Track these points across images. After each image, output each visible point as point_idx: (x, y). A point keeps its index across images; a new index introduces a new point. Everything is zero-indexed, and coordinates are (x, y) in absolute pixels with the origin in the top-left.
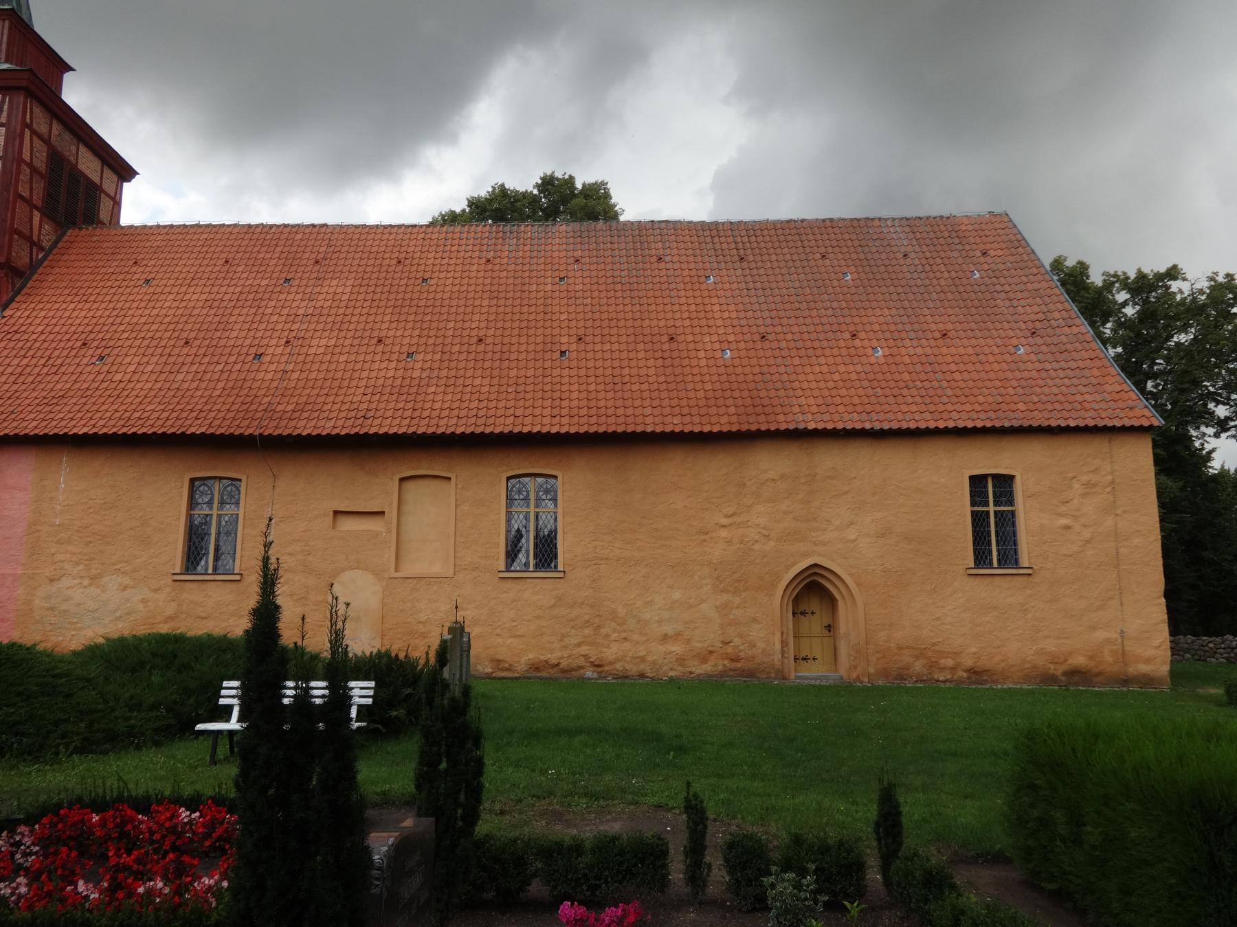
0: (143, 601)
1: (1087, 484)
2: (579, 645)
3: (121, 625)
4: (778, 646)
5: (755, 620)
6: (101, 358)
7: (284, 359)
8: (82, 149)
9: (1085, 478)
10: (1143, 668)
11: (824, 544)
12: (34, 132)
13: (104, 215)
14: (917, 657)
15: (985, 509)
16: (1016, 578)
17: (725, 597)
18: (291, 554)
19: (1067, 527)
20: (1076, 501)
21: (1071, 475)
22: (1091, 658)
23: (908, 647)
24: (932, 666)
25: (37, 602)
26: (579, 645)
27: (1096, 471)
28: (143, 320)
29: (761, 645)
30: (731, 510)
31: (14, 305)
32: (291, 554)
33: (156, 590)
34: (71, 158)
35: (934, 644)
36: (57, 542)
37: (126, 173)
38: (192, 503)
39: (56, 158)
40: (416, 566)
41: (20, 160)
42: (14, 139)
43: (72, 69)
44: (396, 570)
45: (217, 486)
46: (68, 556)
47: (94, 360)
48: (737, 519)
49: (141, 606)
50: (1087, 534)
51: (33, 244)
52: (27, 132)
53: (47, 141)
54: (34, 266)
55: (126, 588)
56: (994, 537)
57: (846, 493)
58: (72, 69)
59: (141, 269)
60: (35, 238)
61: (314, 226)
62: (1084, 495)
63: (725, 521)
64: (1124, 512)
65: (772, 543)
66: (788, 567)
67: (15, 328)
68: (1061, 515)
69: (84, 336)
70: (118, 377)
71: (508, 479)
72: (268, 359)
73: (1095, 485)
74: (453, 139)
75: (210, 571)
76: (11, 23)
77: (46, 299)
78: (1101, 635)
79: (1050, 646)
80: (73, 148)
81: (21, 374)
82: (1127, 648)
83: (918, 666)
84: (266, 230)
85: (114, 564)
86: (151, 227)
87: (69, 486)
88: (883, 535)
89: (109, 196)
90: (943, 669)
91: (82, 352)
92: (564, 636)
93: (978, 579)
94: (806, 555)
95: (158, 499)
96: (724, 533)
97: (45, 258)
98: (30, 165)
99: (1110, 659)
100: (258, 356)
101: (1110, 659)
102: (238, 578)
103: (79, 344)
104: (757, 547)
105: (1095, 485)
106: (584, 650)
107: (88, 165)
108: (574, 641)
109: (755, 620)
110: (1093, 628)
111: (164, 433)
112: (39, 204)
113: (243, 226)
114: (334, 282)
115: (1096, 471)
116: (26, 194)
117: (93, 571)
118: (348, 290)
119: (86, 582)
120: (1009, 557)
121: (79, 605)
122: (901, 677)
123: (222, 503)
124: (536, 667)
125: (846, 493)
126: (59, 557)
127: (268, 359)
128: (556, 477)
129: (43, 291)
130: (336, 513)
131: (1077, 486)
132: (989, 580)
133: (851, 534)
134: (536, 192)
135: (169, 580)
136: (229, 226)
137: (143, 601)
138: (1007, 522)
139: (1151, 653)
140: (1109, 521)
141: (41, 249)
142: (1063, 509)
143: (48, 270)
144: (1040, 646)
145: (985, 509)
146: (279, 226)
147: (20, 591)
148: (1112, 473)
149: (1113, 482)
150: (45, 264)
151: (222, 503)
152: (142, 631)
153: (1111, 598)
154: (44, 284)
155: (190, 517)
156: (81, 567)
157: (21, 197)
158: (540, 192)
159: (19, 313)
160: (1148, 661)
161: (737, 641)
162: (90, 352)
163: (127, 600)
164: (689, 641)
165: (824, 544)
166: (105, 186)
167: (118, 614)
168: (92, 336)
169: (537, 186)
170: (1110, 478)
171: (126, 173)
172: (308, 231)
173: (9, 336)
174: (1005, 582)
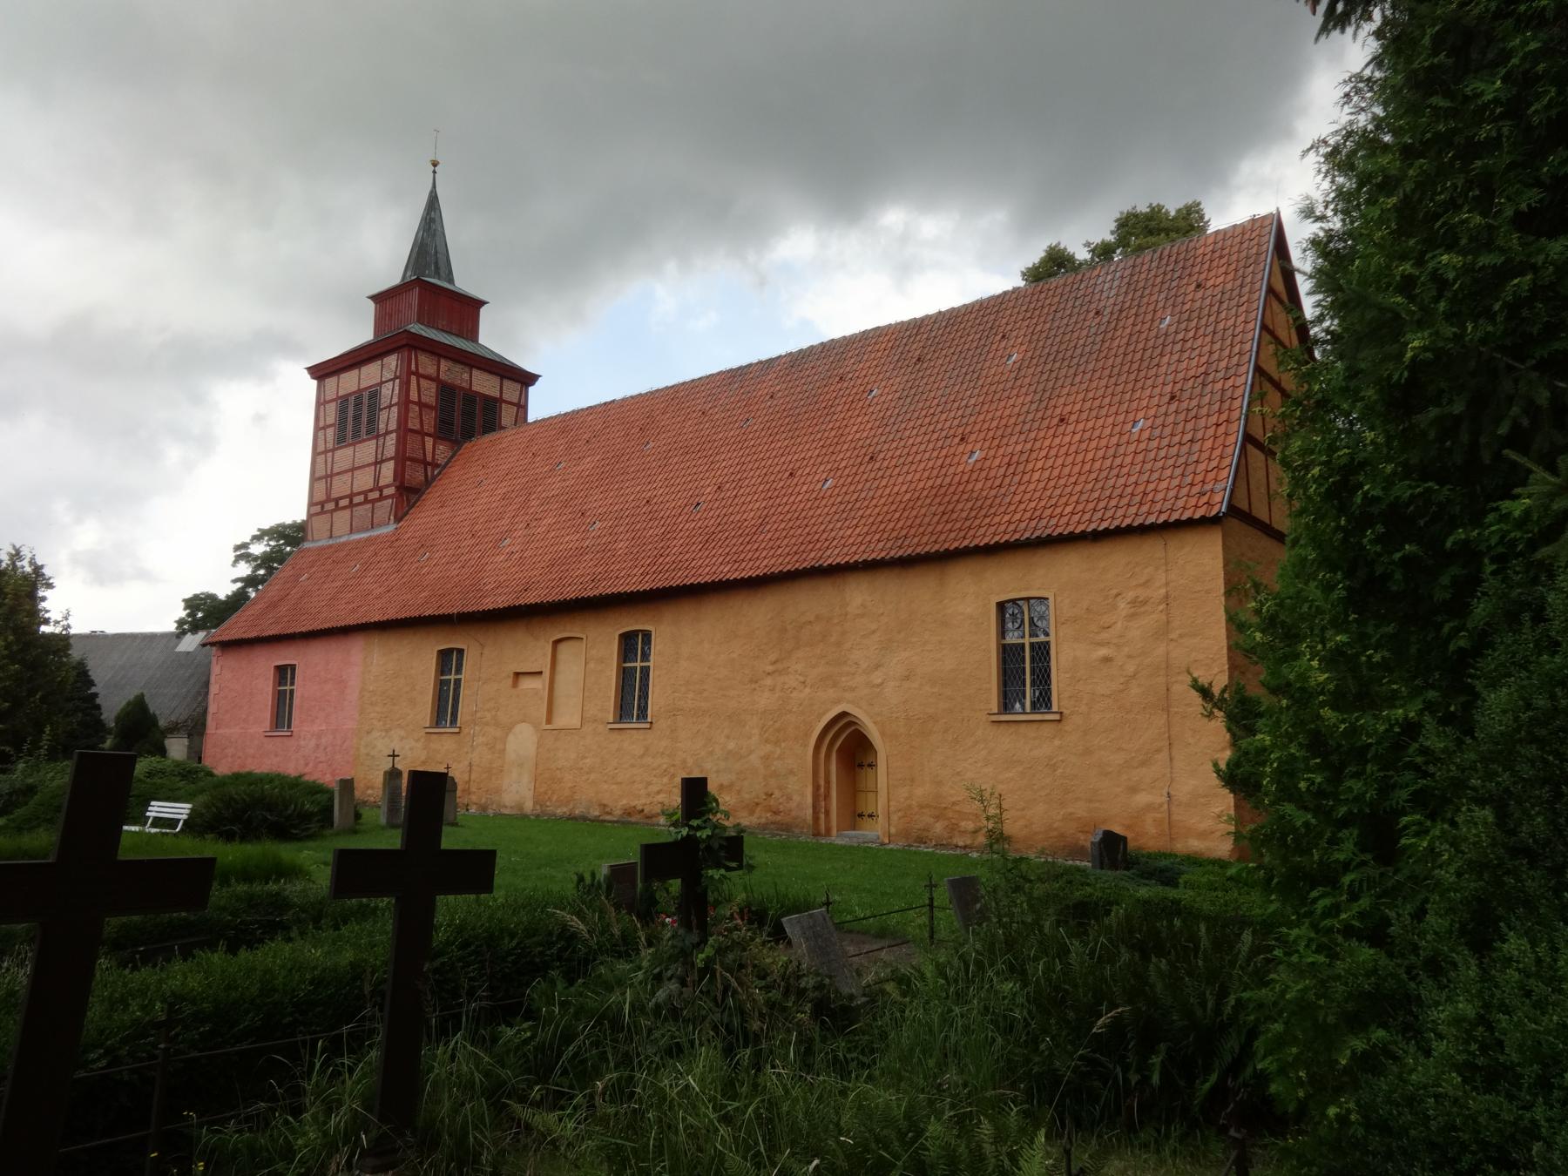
1: (1133, 602)
2: (658, 793)
4: (809, 800)
5: (791, 772)
9: (1131, 595)
10: (1195, 845)
11: (853, 689)
12: (419, 376)
14: (937, 818)
16: (1044, 725)
17: (769, 747)
19: (1107, 660)
20: (1119, 624)
21: (1114, 592)
22: (1128, 827)
23: (928, 806)
24: (953, 828)
26: (658, 793)
27: (1146, 584)
29: (796, 798)
30: (773, 657)
35: (954, 804)
37: (527, 379)
40: (561, 721)
43: (483, 303)
44: (549, 721)
48: (779, 666)
50: (1131, 668)
51: (426, 464)
52: (413, 378)
53: (436, 379)
54: (428, 483)
56: (1024, 675)
57: (874, 632)
58: (483, 303)
60: (429, 459)
62: (1132, 617)
63: (770, 668)
64: (1181, 636)
65: (807, 690)
66: (820, 716)
68: (1101, 644)
69: (960, 430)
73: (1145, 603)
78: (1142, 799)
79: (1080, 809)
80: (466, 376)
81: (1009, 465)
82: (1174, 817)
83: (939, 828)
88: (907, 678)
90: (964, 832)
91: (1061, 429)
92: (649, 784)
93: (1003, 726)
94: (838, 701)
96: (769, 681)
99: (1152, 830)
101: (1152, 830)
103: (1055, 421)
104: (794, 694)
105: (1145, 603)
106: (660, 798)
108: (656, 788)
109: (791, 772)
110: (1133, 790)
112: (432, 430)
115: (1146, 584)
120: (1043, 701)
122: (921, 840)
124: (628, 812)
125: (874, 632)
130: (517, 675)
131: (1122, 605)
132: (1013, 728)
133: (877, 677)
139: (1206, 825)
140: (1161, 650)
141: (437, 466)
142: (1105, 635)
144: (1070, 810)
148: (1167, 584)
149: (1167, 596)
153: (1159, 751)
160: (1203, 835)
161: (777, 794)
162: (1071, 428)
164: (739, 792)
165: (853, 689)
166: (505, 397)
168: (1068, 408)
170: (1163, 591)
171: (527, 379)
174: (1030, 731)
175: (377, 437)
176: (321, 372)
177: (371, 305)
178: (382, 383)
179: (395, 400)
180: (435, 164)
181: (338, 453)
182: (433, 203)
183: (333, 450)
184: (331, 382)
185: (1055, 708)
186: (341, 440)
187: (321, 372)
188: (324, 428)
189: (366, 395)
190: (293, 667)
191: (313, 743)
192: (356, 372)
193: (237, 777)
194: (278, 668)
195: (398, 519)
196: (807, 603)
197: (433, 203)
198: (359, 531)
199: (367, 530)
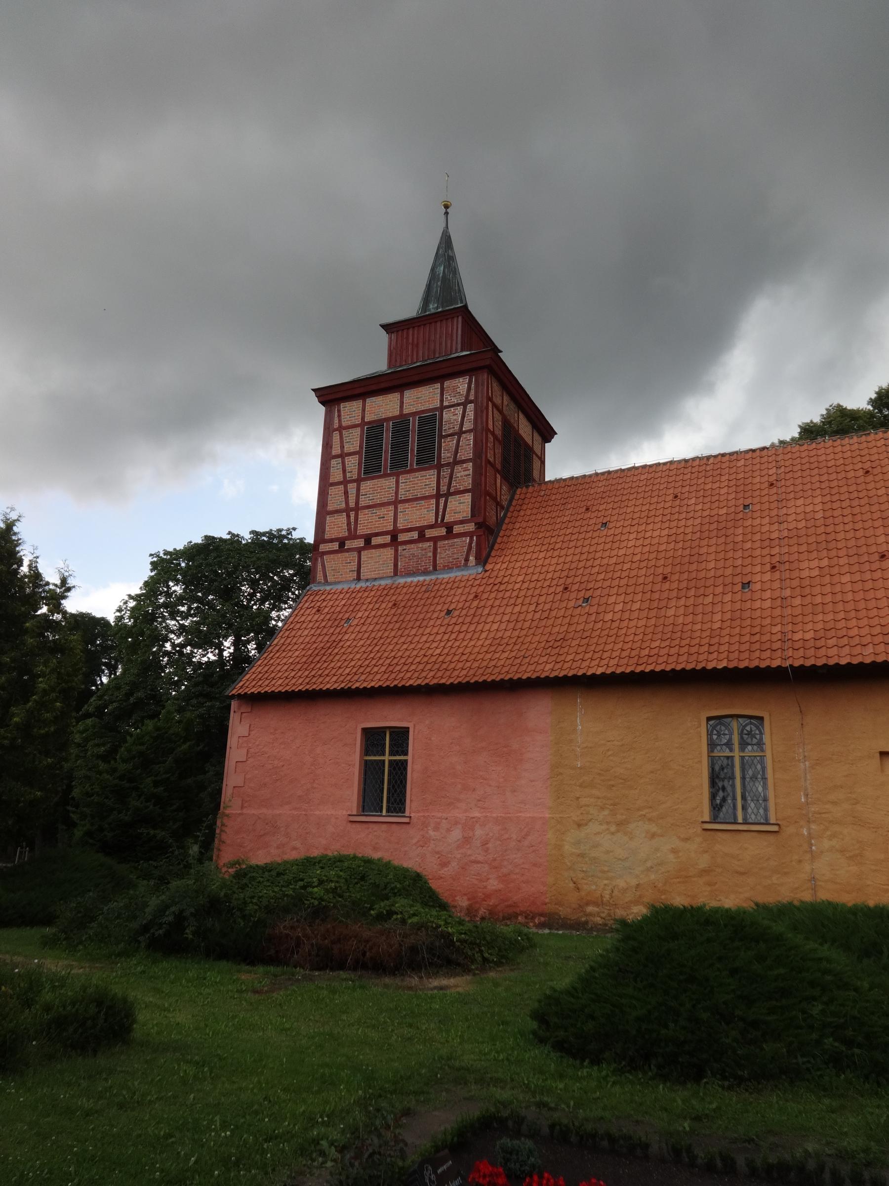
0: (674, 851)
3: (653, 877)
6: (586, 600)
7: (777, 585)
8: (521, 416)
12: (494, 405)
13: (536, 474)
15: (381, 758)
18: (834, 803)
25: (568, 848)
28: (614, 560)
31: (491, 560)
32: (834, 803)
33: (686, 840)
34: (515, 425)
36: (581, 786)
38: (712, 745)
39: (508, 426)
41: (488, 430)
42: (482, 412)
45: (734, 724)
46: (592, 800)
47: (580, 602)
49: (671, 857)
53: (501, 412)
54: (500, 523)
55: (653, 836)
59: (593, 515)
61: (753, 451)
67: (499, 580)
70: (609, 617)
71: (709, 719)
72: (758, 586)
74: (710, 389)
75: (740, 820)
76: (463, 318)
77: (516, 551)
84: (705, 461)
85: (639, 810)
86: (590, 476)
87: (592, 729)
89: (537, 455)
95: (679, 737)
97: (505, 515)
98: (493, 433)
100: (746, 585)
102: (775, 828)
103: (471, 597)
107: (525, 429)
111: (460, 683)
113: (679, 462)
114: (800, 502)
116: (492, 460)
117: (619, 817)
118: (819, 507)
119: (613, 828)
120: (398, 804)
121: (608, 852)
123: (743, 745)
126: (583, 801)
127: (758, 586)
128: (761, 719)
129: (511, 545)
134: (870, 408)
135: (699, 830)
136: (665, 464)
137: (674, 851)
138: (399, 770)
141: (502, 508)
143: (510, 526)
145: (381, 758)
146: (715, 457)
147: (550, 835)
150: (507, 521)
151: (743, 745)
152: (848, 899)
154: (512, 539)
155: (712, 761)
156: (606, 812)
157: (489, 462)
158: (874, 407)
159: (498, 566)
163: (657, 850)
167: (649, 864)
169: (872, 402)
172: (748, 456)
173: (496, 587)
175: (439, 467)
176: (330, 397)
177: (384, 336)
178: (442, 408)
179: (468, 426)
180: (446, 207)
181: (366, 486)
182: (446, 242)
183: (358, 481)
184: (351, 411)
185: (407, 814)
186: (372, 467)
187: (330, 397)
188: (342, 456)
189: (414, 424)
190: (406, 731)
191: (456, 834)
192: (360, 402)
193: (876, 907)
194: (365, 731)
195: (482, 560)
196: (501, 710)
197: (446, 242)
198: (410, 574)
199: (425, 572)
